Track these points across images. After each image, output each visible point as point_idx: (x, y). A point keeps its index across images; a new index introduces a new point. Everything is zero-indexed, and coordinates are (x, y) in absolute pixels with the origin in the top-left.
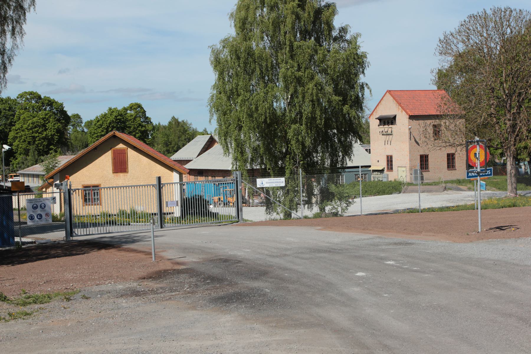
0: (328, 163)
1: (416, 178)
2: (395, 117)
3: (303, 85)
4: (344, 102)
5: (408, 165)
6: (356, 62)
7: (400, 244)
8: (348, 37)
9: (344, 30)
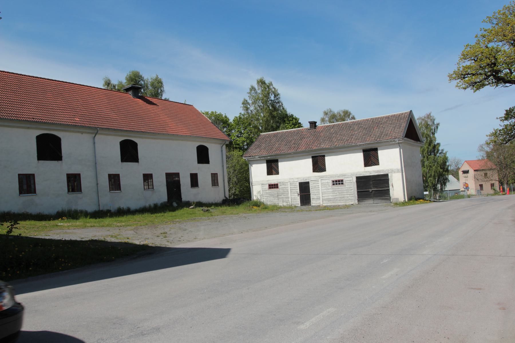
2: (468, 171)
4: (444, 171)
6: (445, 160)
7: (224, 181)
8: (444, 152)
9: (443, 150)
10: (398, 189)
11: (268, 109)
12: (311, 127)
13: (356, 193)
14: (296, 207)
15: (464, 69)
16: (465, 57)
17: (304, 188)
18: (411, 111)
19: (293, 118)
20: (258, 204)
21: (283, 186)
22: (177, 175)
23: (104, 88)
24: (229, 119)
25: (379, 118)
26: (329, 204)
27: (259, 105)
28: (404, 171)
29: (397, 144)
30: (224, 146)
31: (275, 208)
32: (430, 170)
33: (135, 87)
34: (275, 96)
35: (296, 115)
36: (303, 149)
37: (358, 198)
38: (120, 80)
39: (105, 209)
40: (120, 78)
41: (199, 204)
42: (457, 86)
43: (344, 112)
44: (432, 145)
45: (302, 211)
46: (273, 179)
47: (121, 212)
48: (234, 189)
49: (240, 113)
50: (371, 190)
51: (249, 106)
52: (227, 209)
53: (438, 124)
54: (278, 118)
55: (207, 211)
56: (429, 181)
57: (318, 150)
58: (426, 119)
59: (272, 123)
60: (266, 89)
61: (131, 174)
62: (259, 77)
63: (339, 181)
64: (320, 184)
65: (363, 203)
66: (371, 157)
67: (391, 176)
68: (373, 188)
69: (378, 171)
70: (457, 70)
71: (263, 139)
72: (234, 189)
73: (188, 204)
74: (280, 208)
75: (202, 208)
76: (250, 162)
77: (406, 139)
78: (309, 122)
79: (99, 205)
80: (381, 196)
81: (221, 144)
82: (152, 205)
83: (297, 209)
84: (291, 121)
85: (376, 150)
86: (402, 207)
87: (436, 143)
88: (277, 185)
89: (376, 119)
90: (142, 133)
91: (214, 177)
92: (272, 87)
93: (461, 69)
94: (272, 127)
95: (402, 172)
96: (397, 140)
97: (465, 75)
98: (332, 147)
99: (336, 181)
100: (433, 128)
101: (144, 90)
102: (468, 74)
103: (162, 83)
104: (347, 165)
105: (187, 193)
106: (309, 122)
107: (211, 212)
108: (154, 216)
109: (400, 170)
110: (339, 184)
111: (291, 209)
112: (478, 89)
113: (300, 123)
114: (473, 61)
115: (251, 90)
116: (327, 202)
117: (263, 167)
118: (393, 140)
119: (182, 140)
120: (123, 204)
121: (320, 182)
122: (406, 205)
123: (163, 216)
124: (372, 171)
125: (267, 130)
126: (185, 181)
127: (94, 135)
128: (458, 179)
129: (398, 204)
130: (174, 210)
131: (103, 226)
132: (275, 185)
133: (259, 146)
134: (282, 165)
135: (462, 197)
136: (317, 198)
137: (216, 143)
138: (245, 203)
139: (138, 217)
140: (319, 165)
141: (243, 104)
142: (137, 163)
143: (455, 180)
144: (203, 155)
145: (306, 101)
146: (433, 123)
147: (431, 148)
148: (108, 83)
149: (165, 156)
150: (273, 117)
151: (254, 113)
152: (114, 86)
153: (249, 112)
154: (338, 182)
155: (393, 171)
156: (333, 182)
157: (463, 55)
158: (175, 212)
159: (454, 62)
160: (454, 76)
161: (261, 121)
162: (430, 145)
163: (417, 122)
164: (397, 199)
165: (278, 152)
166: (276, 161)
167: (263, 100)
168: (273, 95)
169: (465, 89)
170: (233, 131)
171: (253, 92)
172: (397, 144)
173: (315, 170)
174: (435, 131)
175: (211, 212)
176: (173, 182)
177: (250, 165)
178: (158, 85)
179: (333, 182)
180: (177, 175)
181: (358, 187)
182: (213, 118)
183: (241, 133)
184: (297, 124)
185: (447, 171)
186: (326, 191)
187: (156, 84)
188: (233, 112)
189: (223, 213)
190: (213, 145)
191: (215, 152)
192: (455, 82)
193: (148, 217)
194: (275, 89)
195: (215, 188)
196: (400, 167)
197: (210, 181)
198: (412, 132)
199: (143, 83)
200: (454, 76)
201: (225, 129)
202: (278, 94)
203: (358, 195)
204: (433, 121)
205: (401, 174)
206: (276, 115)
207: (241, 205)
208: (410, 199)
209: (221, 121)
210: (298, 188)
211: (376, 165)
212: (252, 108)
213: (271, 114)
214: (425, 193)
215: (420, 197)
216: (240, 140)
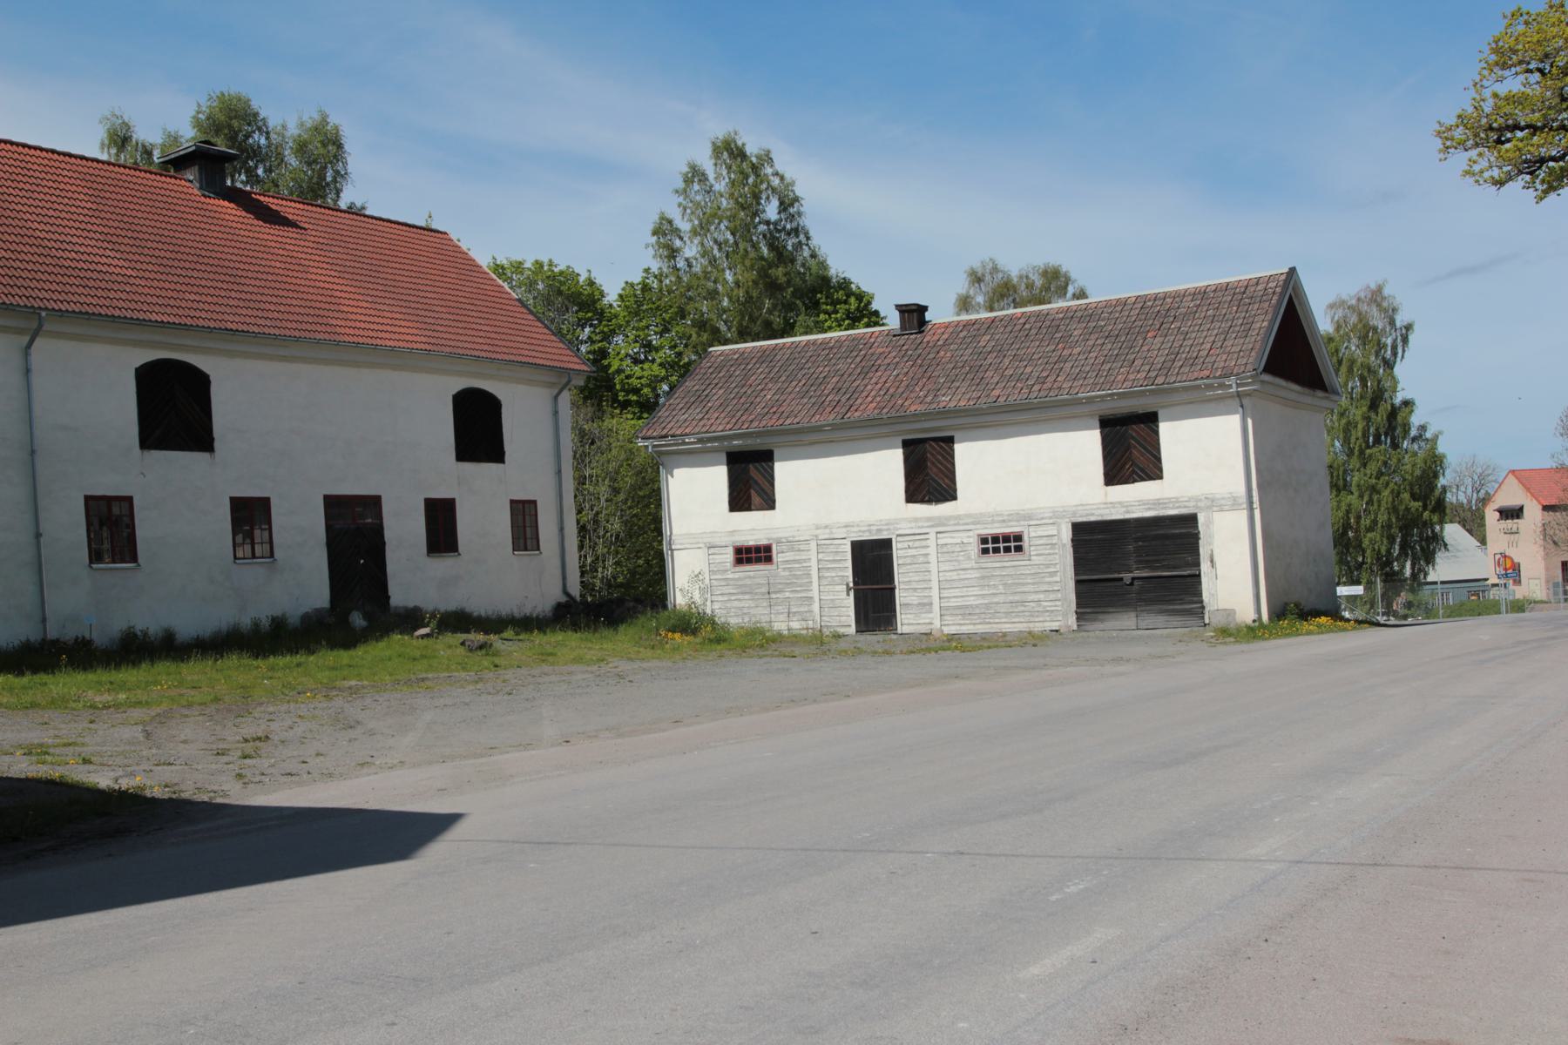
0: (1408, 572)
1: (1556, 594)
2: (1521, 509)
3: (1379, 493)
4: (1425, 507)
5: (1543, 577)
6: (1434, 464)
7: (562, 529)
8: (1428, 435)
9: (1423, 428)
10: (1231, 576)
11: (752, 255)
12: (903, 327)
13: (1071, 585)
14: (837, 636)
15: (1497, 108)
16: (1504, 58)
17: (873, 565)
18: (1293, 271)
19: (849, 294)
20: (690, 624)
21: (790, 556)
22: (374, 503)
23: (105, 157)
24: (602, 295)
25: (1166, 296)
26: (965, 629)
27: (721, 238)
28: (1256, 505)
29: (1231, 396)
30: (566, 398)
31: (759, 641)
32: (1370, 502)
33: (222, 157)
34: (784, 206)
35: (862, 280)
36: (870, 410)
37: (1078, 605)
38: (172, 129)
39: (70, 633)
40: (169, 118)
41: (457, 621)
42: (1467, 173)
43: (1045, 273)
44: (1384, 409)
45: (859, 651)
46: (753, 526)
47: (135, 649)
48: (610, 562)
49: (647, 271)
50: (1127, 577)
51: (678, 243)
52: (568, 642)
53: (1409, 327)
54: (792, 289)
55: (481, 647)
56: (1366, 542)
57: (928, 415)
58: (1364, 308)
59: (770, 312)
60: (747, 178)
61: (180, 501)
62: (719, 130)
63: (1006, 538)
64: (932, 550)
65: (1101, 626)
66: (1130, 448)
67: (1209, 522)
68: (1137, 568)
69: (1158, 503)
70: (1470, 110)
71: (719, 368)
72: (610, 562)
73: (410, 620)
74: (778, 639)
75: (464, 636)
76: (664, 459)
77: (1267, 377)
78: (898, 307)
79: (44, 620)
80: (1169, 602)
81: (551, 385)
82: (265, 623)
83: (843, 645)
84: (839, 302)
85: (1151, 419)
86: (1244, 647)
87: (1398, 400)
88: (768, 549)
89: (1156, 297)
90: (231, 337)
91: (523, 515)
92: (769, 171)
93: (1488, 107)
94: (768, 324)
95: (1251, 509)
96: (1232, 381)
97: (1500, 130)
98: (982, 404)
99: (995, 539)
100: (1389, 341)
101: (269, 171)
102: (1517, 127)
103: (340, 146)
104: (1039, 476)
105: (412, 575)
106: (898, 307)
107: (497, 654)
108: (262, 664)
109: (1244, 500)
110: (1007, 550)
111: (819, 643)
112: (1551, 188)
113: (876, 313)
114: (1537, 76)
115: (688, 181)
116: (958, 619)
117: (717, 477)
118: (1215, 382)
119: (395, 368)
120: (147, 618)
121: (932, 542)
122: (1262, 638)
123: (299, 665)
124: (1134, 500)
125: (744, 335)
126: (404, 530)
127: (27, 339)
128: (1483, 541)
129: (1232, 633)
130: (349, 640)
131: (34, 705)
132: (758, 549)
133: (700, 398)
134: (788, 474)
135: (1493, 608)
136: (915, 610)
137: (530, 382)
138: (642, 619)
139: (195, 671)
140: (929, 478)
141: (655, 233)
142: (206, 455)
143: (1472, 542)
144: (478, 426)
145: (901, 227)
146: (1392, 322)
147: (1380, 418)
148: (120, 139)
149: (325, 425)
150: (773, 287)
151: (697, 269)
152: (148, 153)
153: (681, 264)
154: (1004, 544)
155: (1214, 503)
156: (984, 541)
157: (1497, 50)
158: (352, 652)
159: (1462, 84)
160: (1459, 133)
161: (725, 303)
162: (1374, 406)
163: (1324, 323)
164: (1230, 613)
165: (770, 422)
166: (766, 457)
167: (732, 218)
168: (775, 203)
169: (1500, 183)
170: (619, 339)
171: (696, 187)
172: (1231, 396)
173: (912, 496)
174: (1395, 354)
175: (497, 654)
176: (354, 530)
177: (662, 471)
178: (324, 154)
179: (984, 541)
180: (374, 503)
181: (1080, 562)
182: (540, 286)
183: (648, 346)
184: (863, 313)
185: (1440, 507)
186: (954, 576)
187: (316, 148)
188: (616, 262)
189: (545, 656)
190: (522, 389)
191: (527, 416)
192: (1460, 159)
193: (237, 670)
194: (782, 178)
195: (525, 558)
196: (1241, 489)
197: (505, 533)
198: (1292, 354)
199: (263, 141)
200: (1459, 133)
201: (587, 330)
202: (796, 199)
203: (1079, 595)
204: (1390, 314)
205: (1244, 514)
206: (783, 280)
207: (622, 628)
208: (1279, 613)
209: (569, 300)
210: (849, 564)
211: (1151, 478)
212: (691, 250)
213: (763, 273)
214: (1343, 591)
215: (1322, 607)
216: (639, 375)
